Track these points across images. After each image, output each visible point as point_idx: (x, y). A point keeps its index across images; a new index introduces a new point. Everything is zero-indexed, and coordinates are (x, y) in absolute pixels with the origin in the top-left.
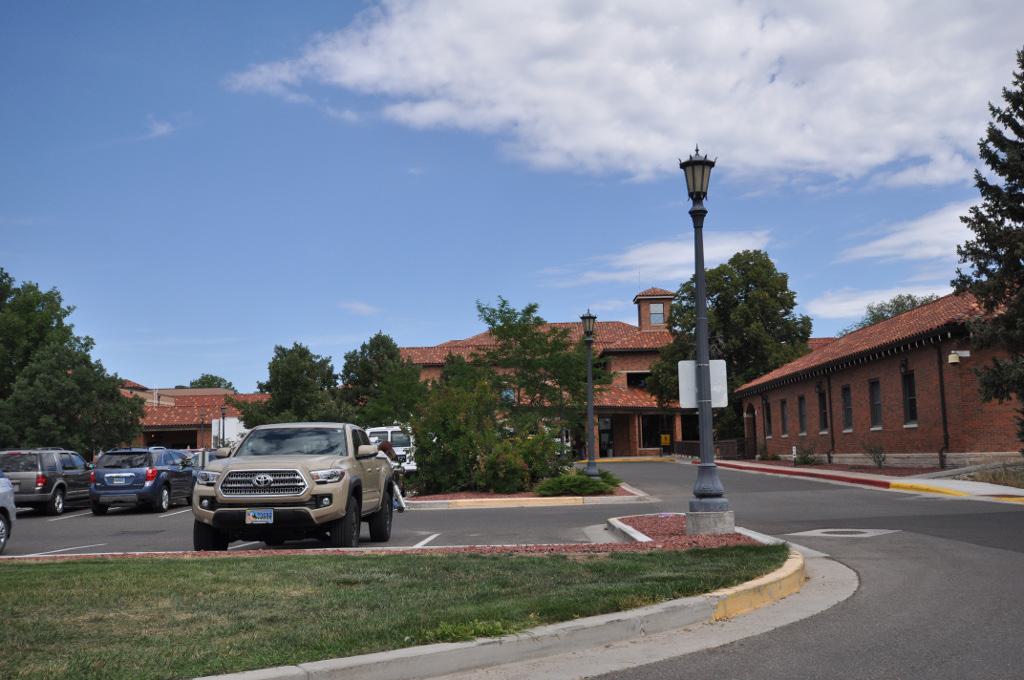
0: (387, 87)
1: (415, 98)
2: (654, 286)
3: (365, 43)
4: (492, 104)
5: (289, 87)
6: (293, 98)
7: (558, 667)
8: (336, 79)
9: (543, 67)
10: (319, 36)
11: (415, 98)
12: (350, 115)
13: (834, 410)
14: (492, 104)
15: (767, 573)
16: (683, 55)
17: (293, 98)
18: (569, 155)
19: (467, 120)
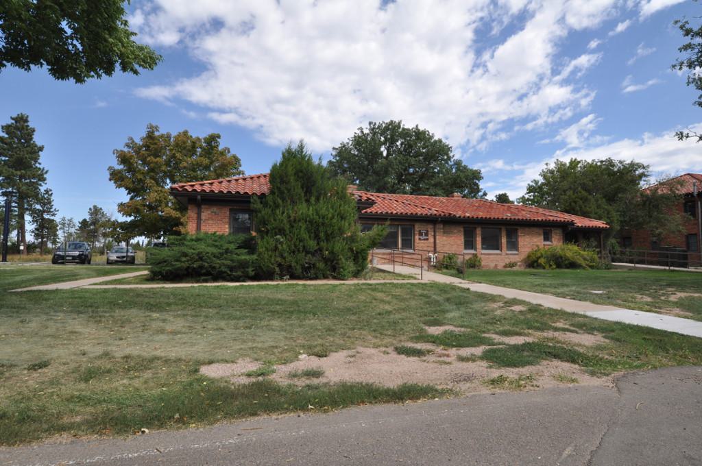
0: (211, 105)
1: (222, 111)
2: (525, 31)
3: (204, 86)
4: (253, 118)
5: (167, 99)
6: (169, 104)
7: (254, 340)
8: (189, 99)
9: (278, 107)
10: (185, 79)
11: (222, 111)
12: (192, 115)
13: (511, 256)
14: (253, 118)
15: (413, 356)
16: (333, 109)
17: (169, 104)
18: (281, 141)
19: (243, 123)
